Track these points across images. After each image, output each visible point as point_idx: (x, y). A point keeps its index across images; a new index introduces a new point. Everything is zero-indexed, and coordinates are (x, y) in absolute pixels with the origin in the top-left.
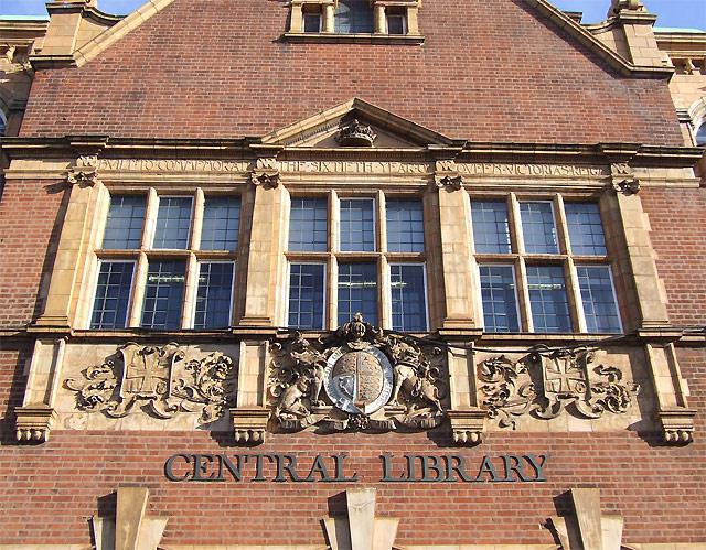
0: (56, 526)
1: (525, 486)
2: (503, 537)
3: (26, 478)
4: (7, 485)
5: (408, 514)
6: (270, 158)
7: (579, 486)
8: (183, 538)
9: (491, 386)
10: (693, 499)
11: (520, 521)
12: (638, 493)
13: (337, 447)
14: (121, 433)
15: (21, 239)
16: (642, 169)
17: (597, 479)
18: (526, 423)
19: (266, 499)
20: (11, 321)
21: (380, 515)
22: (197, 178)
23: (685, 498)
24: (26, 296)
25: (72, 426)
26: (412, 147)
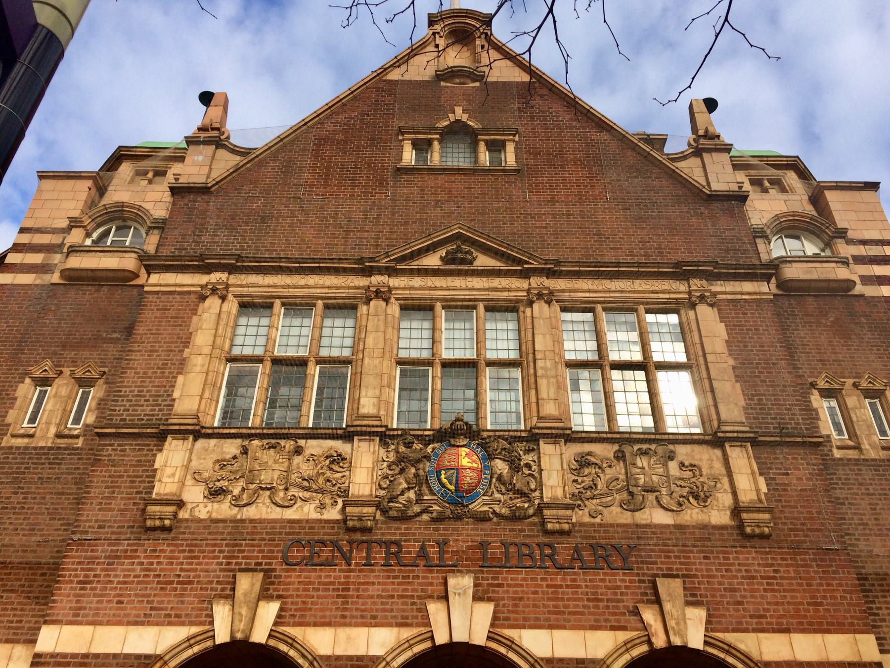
0: (179, 609)
1: (612, 574)
2: (593, 623)
3: (152, 564)
4: (133, 570)
5: (503, 599)
6: (382, 274)
7: (664, 576)
8: (297, 620)
9: (580, 479)
10: (773, 590)
11: (608, 607)
12: (720, 583)
13: (440, 535)
14: (243, 521)
15: (157, 345)
16: (719, 283)
17: (681, 569)
18: (616, 515)
19: (373, 583)
20: (145, 418)
21: (477, 598)
22: (318, 292)
23: (765, 590)
24: (159, 396)
25: (197, 514)
26: (512, 266)
